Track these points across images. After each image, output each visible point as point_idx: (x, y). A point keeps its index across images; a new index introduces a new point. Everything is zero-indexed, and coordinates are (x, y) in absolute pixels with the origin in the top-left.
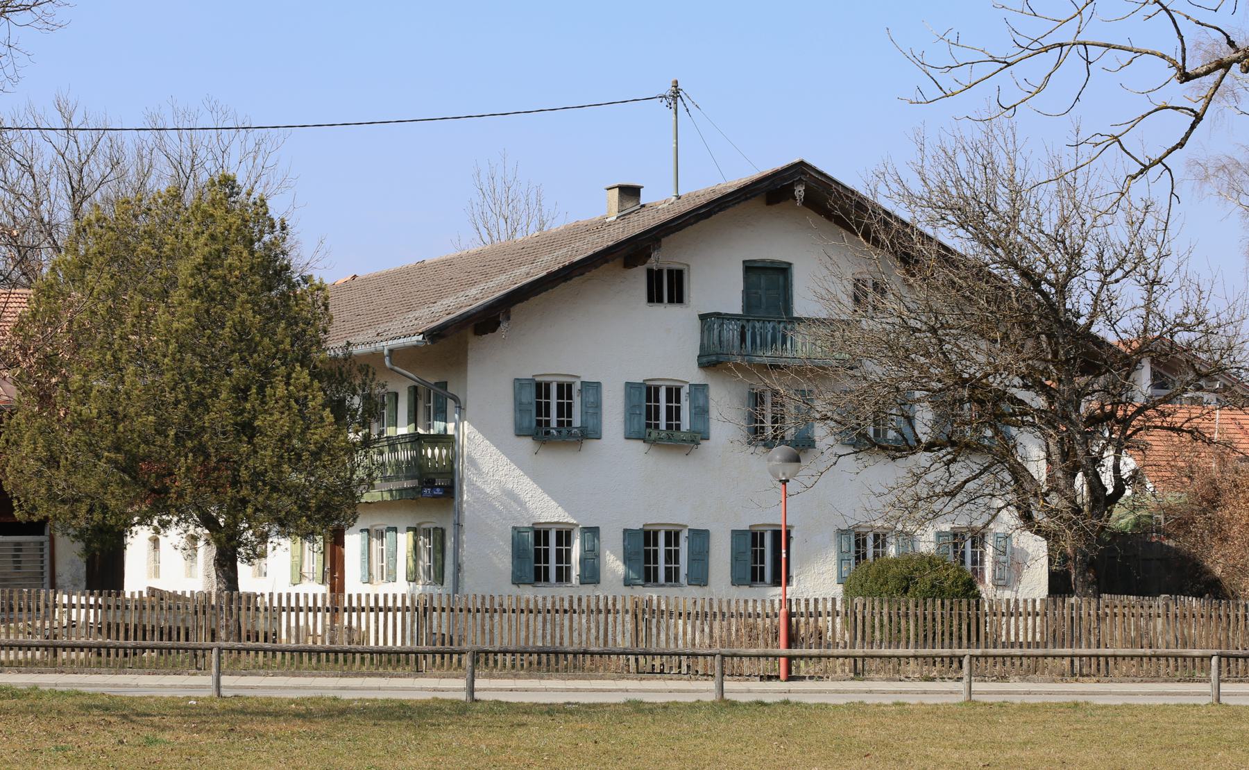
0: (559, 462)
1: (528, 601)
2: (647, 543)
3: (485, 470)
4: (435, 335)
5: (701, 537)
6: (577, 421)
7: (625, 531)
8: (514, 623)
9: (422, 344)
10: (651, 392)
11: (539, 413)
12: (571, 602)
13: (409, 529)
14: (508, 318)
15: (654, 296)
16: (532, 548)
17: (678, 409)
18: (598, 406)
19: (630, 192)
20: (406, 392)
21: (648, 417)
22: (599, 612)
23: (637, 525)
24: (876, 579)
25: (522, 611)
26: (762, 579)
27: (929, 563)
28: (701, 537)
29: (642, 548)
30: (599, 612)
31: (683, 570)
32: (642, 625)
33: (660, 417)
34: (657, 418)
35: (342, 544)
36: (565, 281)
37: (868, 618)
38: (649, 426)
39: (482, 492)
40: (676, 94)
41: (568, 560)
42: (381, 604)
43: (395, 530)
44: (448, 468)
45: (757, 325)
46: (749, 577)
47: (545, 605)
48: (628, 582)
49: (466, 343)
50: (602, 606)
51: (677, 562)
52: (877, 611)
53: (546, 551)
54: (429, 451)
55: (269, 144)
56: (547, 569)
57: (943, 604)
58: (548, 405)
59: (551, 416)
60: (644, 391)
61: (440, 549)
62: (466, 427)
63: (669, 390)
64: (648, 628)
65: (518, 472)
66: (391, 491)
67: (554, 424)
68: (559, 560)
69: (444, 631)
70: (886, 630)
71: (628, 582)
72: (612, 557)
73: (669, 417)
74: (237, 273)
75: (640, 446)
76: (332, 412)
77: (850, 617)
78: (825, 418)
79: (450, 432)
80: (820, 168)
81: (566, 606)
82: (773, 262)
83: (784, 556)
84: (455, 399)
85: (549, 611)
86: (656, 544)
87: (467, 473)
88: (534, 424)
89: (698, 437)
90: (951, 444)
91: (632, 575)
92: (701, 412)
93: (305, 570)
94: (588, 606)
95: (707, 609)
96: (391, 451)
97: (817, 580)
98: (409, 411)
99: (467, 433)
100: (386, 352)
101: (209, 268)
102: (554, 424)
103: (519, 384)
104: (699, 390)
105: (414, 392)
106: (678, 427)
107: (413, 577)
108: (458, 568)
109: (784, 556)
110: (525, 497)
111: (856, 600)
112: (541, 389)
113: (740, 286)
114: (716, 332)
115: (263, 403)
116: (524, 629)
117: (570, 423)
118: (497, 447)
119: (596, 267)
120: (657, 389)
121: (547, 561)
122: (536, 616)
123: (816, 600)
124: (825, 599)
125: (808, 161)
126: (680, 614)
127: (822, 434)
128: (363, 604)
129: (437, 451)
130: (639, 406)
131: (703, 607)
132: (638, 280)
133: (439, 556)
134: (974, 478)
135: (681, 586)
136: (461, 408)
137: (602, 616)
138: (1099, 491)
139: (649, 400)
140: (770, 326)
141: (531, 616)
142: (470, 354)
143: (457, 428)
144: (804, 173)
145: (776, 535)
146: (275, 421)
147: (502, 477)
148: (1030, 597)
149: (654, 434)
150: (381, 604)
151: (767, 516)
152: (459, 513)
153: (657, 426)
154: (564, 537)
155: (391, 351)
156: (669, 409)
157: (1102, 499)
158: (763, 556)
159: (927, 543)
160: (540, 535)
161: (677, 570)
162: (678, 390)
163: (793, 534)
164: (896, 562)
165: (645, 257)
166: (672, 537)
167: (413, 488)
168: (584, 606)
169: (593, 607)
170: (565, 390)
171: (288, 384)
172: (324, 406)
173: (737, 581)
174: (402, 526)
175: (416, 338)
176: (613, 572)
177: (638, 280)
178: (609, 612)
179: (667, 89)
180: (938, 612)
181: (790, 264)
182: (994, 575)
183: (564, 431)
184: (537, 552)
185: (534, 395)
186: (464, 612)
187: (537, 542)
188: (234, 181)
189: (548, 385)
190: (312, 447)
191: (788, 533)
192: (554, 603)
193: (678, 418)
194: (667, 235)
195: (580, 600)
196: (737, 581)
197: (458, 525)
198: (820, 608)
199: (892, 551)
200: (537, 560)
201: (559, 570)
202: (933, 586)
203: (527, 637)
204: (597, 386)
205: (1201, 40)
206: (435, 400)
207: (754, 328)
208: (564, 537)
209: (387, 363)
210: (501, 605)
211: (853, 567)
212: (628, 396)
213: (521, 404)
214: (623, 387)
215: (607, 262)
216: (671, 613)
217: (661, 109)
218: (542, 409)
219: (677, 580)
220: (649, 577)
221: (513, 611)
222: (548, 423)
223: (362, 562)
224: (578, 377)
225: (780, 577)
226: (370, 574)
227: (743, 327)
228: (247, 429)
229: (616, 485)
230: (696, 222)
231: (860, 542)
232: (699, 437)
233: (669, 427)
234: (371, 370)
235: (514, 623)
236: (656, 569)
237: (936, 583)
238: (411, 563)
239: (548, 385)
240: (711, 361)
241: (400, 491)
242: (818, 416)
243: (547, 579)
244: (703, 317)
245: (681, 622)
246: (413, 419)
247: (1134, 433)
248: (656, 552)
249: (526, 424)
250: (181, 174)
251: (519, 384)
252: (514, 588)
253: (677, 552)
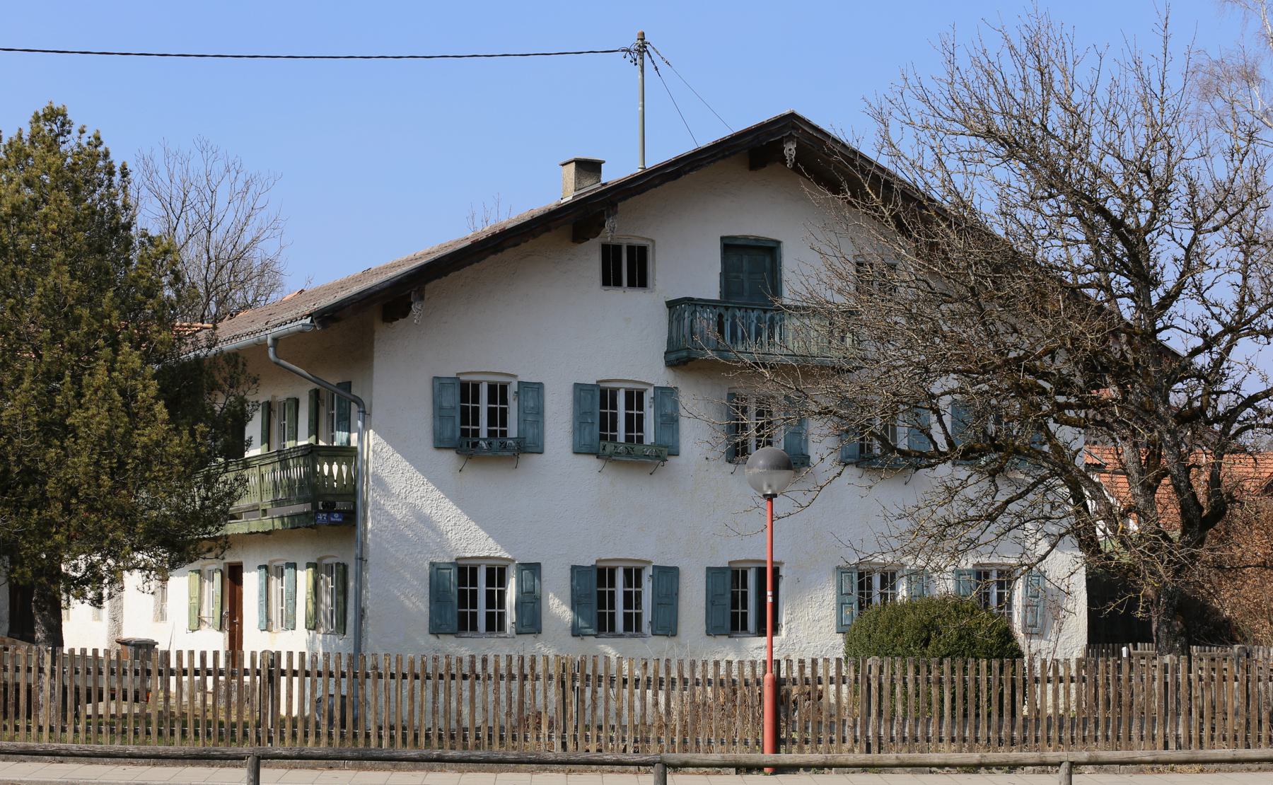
0: (491, 483)
1: (412, 662)
2: (601, 582)
3: (396, 490)
4: (326, 317)
5: (668, 577)
6: (513, 430)
7: (574, 568)
8: (393, 694)
9: (309, 329)
10: (606, 396)
11: (464, 421)
12: (473, 663)
13: (308, 565)
14: (422, 298)
15: (610, 278)
16: (454, 590)
17: (640, 417)
18: (539, 412)
19: (588, 167)
20: (307, 398)
21: (603, 427)
22: (512, 677)
23: (589, 562)
24: (888, 629)
25: (404, 676)
26: (745, 628)
27: (955, 607)
28: (668, 577)
29: (595, 589)
30: (512, 677)
31: (647, 616)
32: (572, 697)
33: (618, 428)
34: (614, 428)
35: (241, 583)
36: (495, 253)
37: (886, 686)
38: (603, 438)
39: (391, 518)
40: (642, 48)
41: (502, 604)
42: (210, 665)
43: (294, 566)
44: (351, 489)
45: (738, 313)
46: (728, 625)
47: (436, 668)
48: (576, 632)
49: (373, 332)
50: (515, 671)
51: (639, 605)
52: (898, 676)
53: (474, 593)
54: (326, 467)
55: (260, 186)
56: (474, 615)
57: (989, 667)
58: (476, 411)
59: (481, 426)
60: (598, 394)
61: (342, 590)
62: (372, 437)
63: (629, 394)
64: (581, 701)
65: (437, 494)
66: (282, 517)
67: (484, 433)
68: (490, 604)
70: (911, 702)
71: (576, 632)
72: (557, 601)
73: (629, 428)
74: (54, 226)
75: (591, 463)
76: (166, 406)
77: (862, 685)
78: (825, 412)
79: (354, 444)
80: (815, 122)
81: (466, 670)
82: (757, 239)
83: (769, 599)
84: (359, 402)
85: (441, 677)
86: (612, 584)
87: (371, 495)
88: (458, 434)
89: (666, 452)
90: (986, 451)
91: (581, 623)
92: (669, 422)
93: (204, 613)
94: (496, 670)
95: (662, 674)
96: (283, 469)
97: (811, 630)
98: (310, 420)
99: (372, 444)
100: (269, 342)
101: (20, 221)
102: (484, 433)
103: (439, 384)
104: (665, 394)
105: (316, 396)
106: (640, 439)
107: (313, 625)
108: (361, 614)
109: (769, 599)
110: (444, 525)
111: (869, 661)
112: (468, 391)
113: (718, 267)
114: (687, 322)
115: (79, 395)
116: (407, 702)
117: (504, 433)
118: (411, 462)
119: (535, 237)
120: (614, 393)
121: (474, 605)
122: (424, 683)
123: (814, 662)
124: (826, 660)
125: (801, 112)
126: (625, 681)
127: (821, 442)
128: (185, 665)
129: (335, 467)
130: (592, 413)
131: (656, 672)
132: (590, 260)
133: (341, 598)
134: (1020, 496)
135: (644, 636)
136: (365, 414)
137: (515, 684)
138: (1194, 511)
139: (603, 406)
140: (754, 315)
141: (418, 683)
142: (378, 347)
143: (360, 439)
144: (796, 128)
145: (761, 572)
146: (94, 418)
147: (416, 499)
149: (610, 447)
150: (210, 665)
151: (748, 549)
152: (363, 545)
153: (614, 438)
154: (497, 575)
155: (275, 340)
156: (629, 418)
157: (1197, 521)
158: (745, 599)
159: (945, 586)
160: (466, 572)
161: (639, 616)
162: (640, 394)
163: (783, 572)
164: (911, 606)
165: (597, 226)
166: (633, 575)
167: (306, 514)
168: (491, 670)
169: (503, 671)
170: (498, 392)
171: (111, 370)
172: (157, 398)
173: (713, 630)
174: (301, 563)
175: (303, 321)
176: (558, 619)
177: (590, 260)
178: (525, 677)
179: (632, 42)
180: (983, 677)
181: (779, 243)
182: (1025, 618)
183: (496, 443)
184: (462, 594)
185: (458, 398)
186: (324, 677)
187: (462, 581)
188: (65, 116)
189: (476, 386)
190: (139, 452)
191: (776, 572)
192: (449, 665)
193: (640, 429)
194: (625, 198)
195: (485, 661)
196: (713, 630)
197: (361, 560)
198: (821, 672)
199: (902, 591)
200: (462, 603)
201: (490, 616)
202: (961, 637)
203: (412, 712)
204: (538, 387)
205: (1201, 62)
206: (339, 405)
207: (734, 317)
208: (497, 575)
209: (271, 355)
210: (375, 668)
211: (856, 612)
212: (577, 400)
213: (441, 408)
214: (571, 388)
215: (548, 230)
216: (612, 680)
217: (625, 68)
218: (468, 416)
219: (639, 628)
220: (604, 626)
221: (392, 676)
222: (476, 433)
223: (260, 605)
224: (515, 376)
225: (767, 624)
226: (268, 619)
227: (720, 316)
228: (56, 429)
229: (563, 511)
230: (660, 184)
231: (864, 582)
232: (666, 452)
233: (629, 439)
234: (240, 360)
235: (393, 694)
236: (612, 616)
237: (964, 633)
238: (311, 607)
239: (476, 386)
240: (680, 358)
241: (291, 517)
242: (813, 407)
243: (474, 628)
244: (671, 305)
245: (626, 692)
246: (314, 430)
247: (1239, 433)
248: (612, 594)
249: (448, 433)
250: (172, 215)
251: (439, 384)
252: (433, 639)
253: (639, 595)
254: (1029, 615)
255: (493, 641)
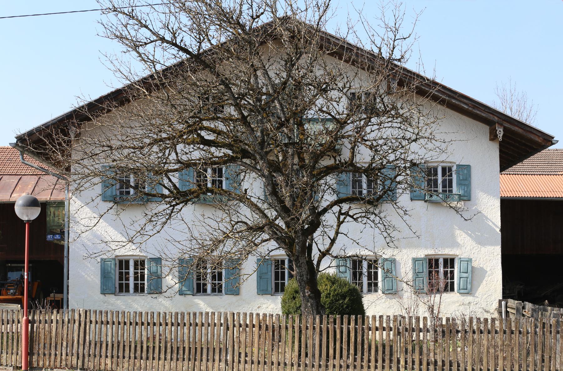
48: (181, 293)
91: (184, 289)
128: (421, 326)
254: (242, 177)
255: (136, 297)
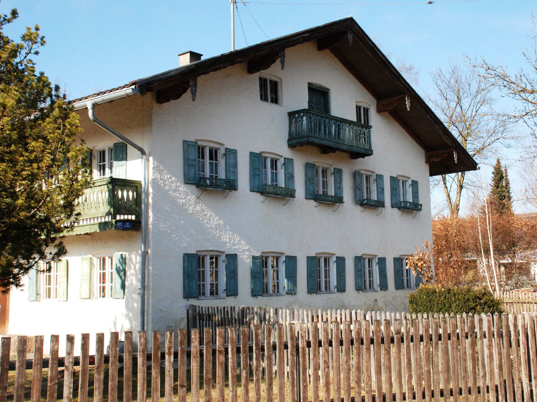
4: (144, 86)
23: (313, 254)
54: (120, 193)
69: (497, 382)
104: (288, 162)
125: (355, 19)
148: (31, 333)
155: (95, 106)
177: (252, 83)
213: (188, 159)
240: (295, 142)
244: (291, 115)
